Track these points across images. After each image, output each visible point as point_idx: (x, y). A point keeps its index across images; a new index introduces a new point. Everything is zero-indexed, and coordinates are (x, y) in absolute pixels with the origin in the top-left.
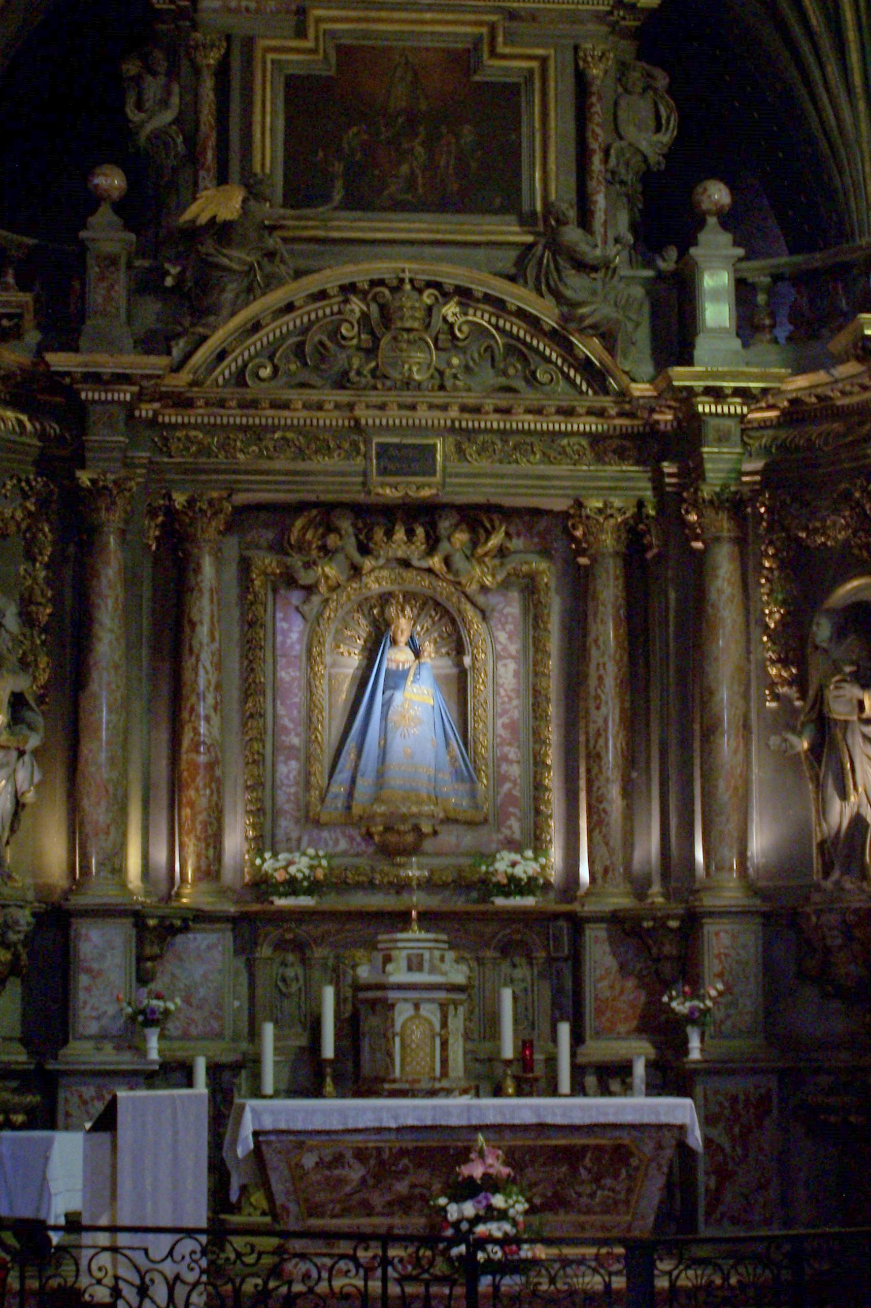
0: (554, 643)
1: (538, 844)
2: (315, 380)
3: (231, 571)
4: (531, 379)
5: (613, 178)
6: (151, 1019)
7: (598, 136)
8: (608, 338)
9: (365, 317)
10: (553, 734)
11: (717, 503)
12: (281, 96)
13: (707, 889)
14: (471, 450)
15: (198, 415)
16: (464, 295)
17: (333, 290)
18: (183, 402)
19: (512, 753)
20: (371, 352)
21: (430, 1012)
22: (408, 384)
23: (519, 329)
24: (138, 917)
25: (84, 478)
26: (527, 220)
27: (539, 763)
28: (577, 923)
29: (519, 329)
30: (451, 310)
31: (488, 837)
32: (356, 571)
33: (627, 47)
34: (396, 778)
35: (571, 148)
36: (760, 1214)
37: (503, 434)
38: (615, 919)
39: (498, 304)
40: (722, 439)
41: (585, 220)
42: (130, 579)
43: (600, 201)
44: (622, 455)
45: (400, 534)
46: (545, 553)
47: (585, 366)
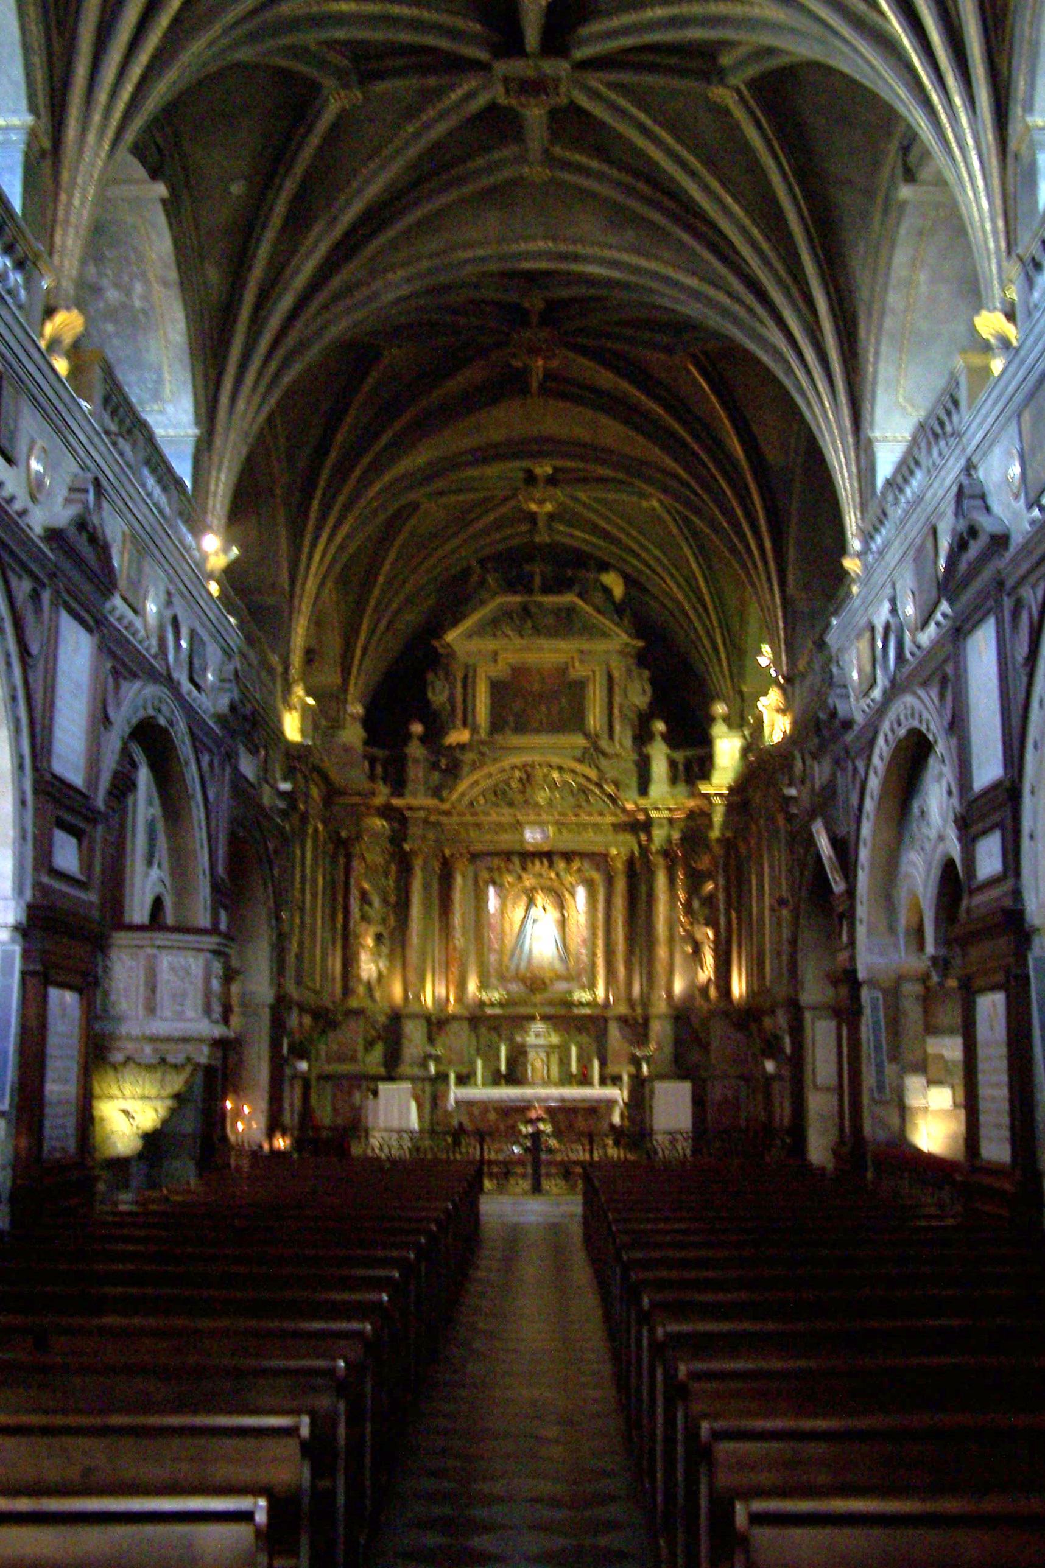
0: (601, 906)
1: (592, 986)
2: (501, 803)
3: (470, 882)
4: (587, 800)
5: (623, 716)
6: (429, 1056)
7: (617, 699)
8: (617, 784)
9: (521, 780)
10: (600, 943)
11: (658, 852)
12: (584, 547)
13: (101, 1018)
14: (564, 831)
15: (455, 819)
16: (560, 769)
17: (507, 767)
18: (448, 813)
19: (583, 951)
20: (523, 792)
21: (543, 1055)
22: (537, 804)
23: (582, 781)
24: (428, 1019)
25: (406, 847)
26: (587, 735)
27: (594, 954)
28: (606, 1020)
29: (582, 781)
30: (555, 775)
31: (574, 985)
32: (520, 878)
33: (631, 661)
34: (535, 962)
35: (605, 705)
36: (168, 981)
37: (577, 824)
38: (623, 1020)
39: (573, 771)
40: (661, 826)
41: (611, 736)
42: (426, 886)
43: (617, 728)
44: (625, 830)
45: (537, 863)
46: (598, 869)
47: (610, 796)
